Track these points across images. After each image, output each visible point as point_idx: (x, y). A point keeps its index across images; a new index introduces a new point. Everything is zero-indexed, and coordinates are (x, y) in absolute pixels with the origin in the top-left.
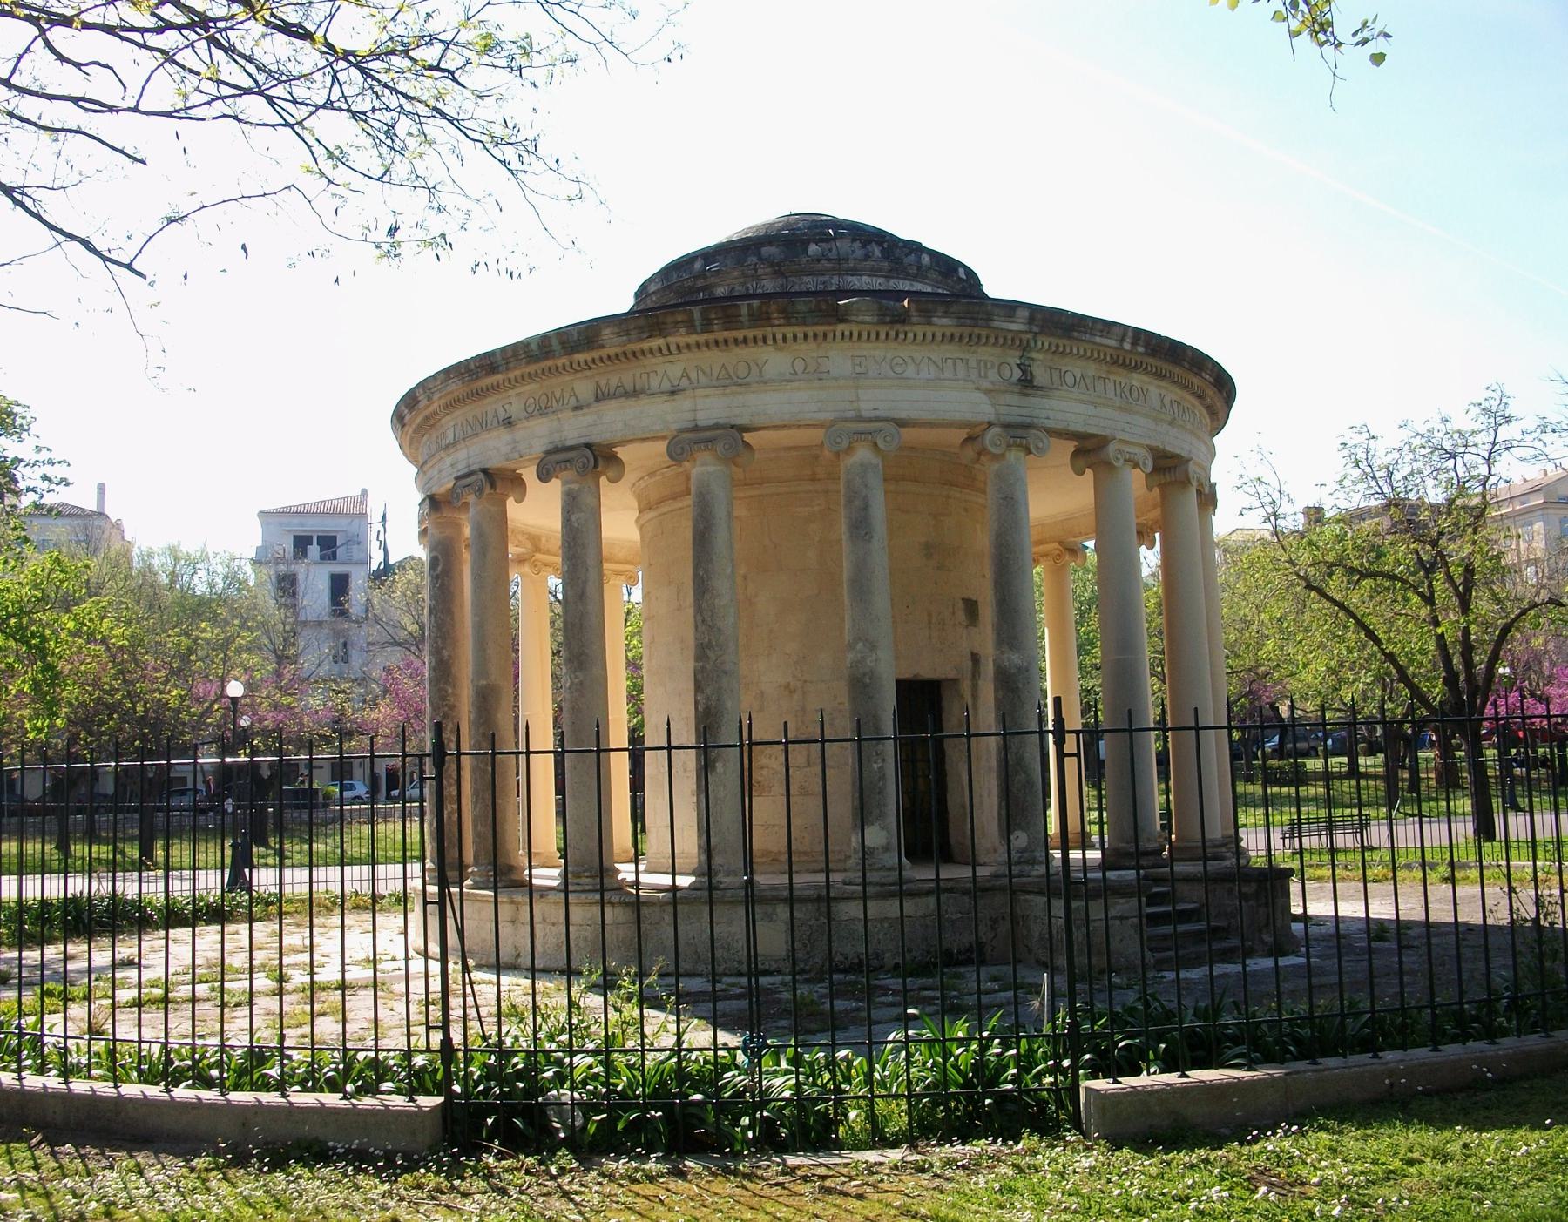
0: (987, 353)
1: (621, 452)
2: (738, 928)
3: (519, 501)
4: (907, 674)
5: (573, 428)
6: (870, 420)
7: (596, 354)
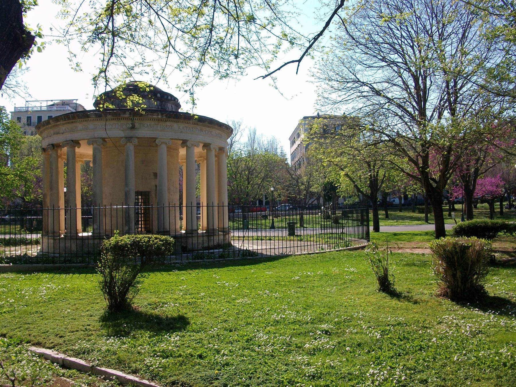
0: (123, 122)
1: (80, 142)
2: (69, 245)
3: (79, 148)
4: (137, 191)
5: (69, 136)
6: (96, 138)
7: (50, 126)
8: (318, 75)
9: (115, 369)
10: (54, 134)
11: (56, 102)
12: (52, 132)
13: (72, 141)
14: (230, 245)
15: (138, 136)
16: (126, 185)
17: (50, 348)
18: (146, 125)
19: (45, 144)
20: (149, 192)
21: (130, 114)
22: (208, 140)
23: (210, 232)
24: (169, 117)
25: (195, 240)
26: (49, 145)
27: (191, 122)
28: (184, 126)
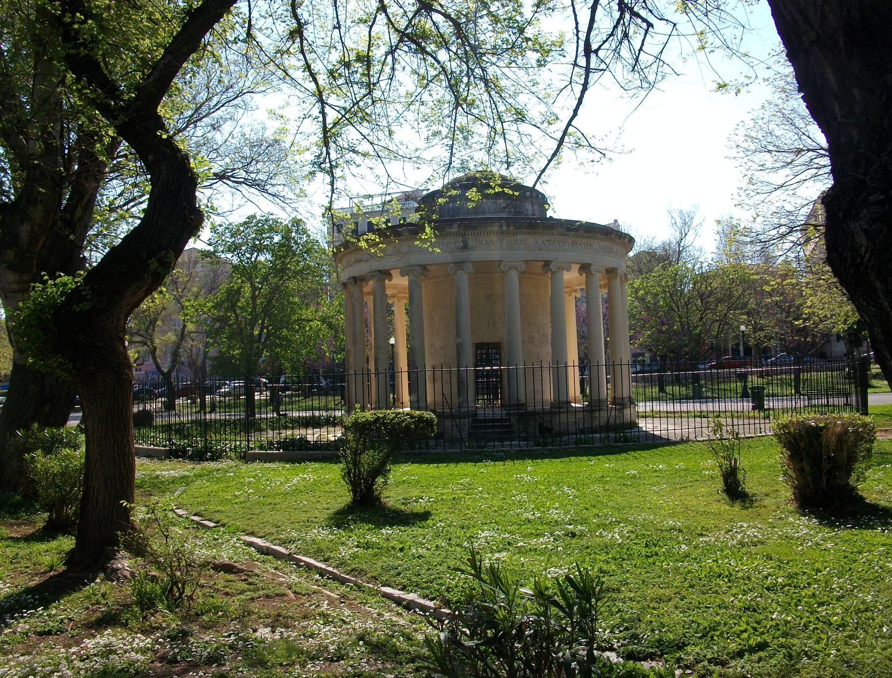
1: (392, 272)
8: (745, 145)
9: (310, 557)
10: (356, 262)
11: (394, 196)
12: (353, 260)
13: (380, 271)
14: (633, 425)
15: (474, 260)
16: (458, 334)
17: (260, 537)
18: (484, 242)
19: (344, 277)
20: (499, 344)
21: (459, 227)
22: (586, 259)
23: (594, 405)
24: (519, 228)
25: (564, 417)
26: (349, 278)
27: (555, 231)
28: (544, 239)
